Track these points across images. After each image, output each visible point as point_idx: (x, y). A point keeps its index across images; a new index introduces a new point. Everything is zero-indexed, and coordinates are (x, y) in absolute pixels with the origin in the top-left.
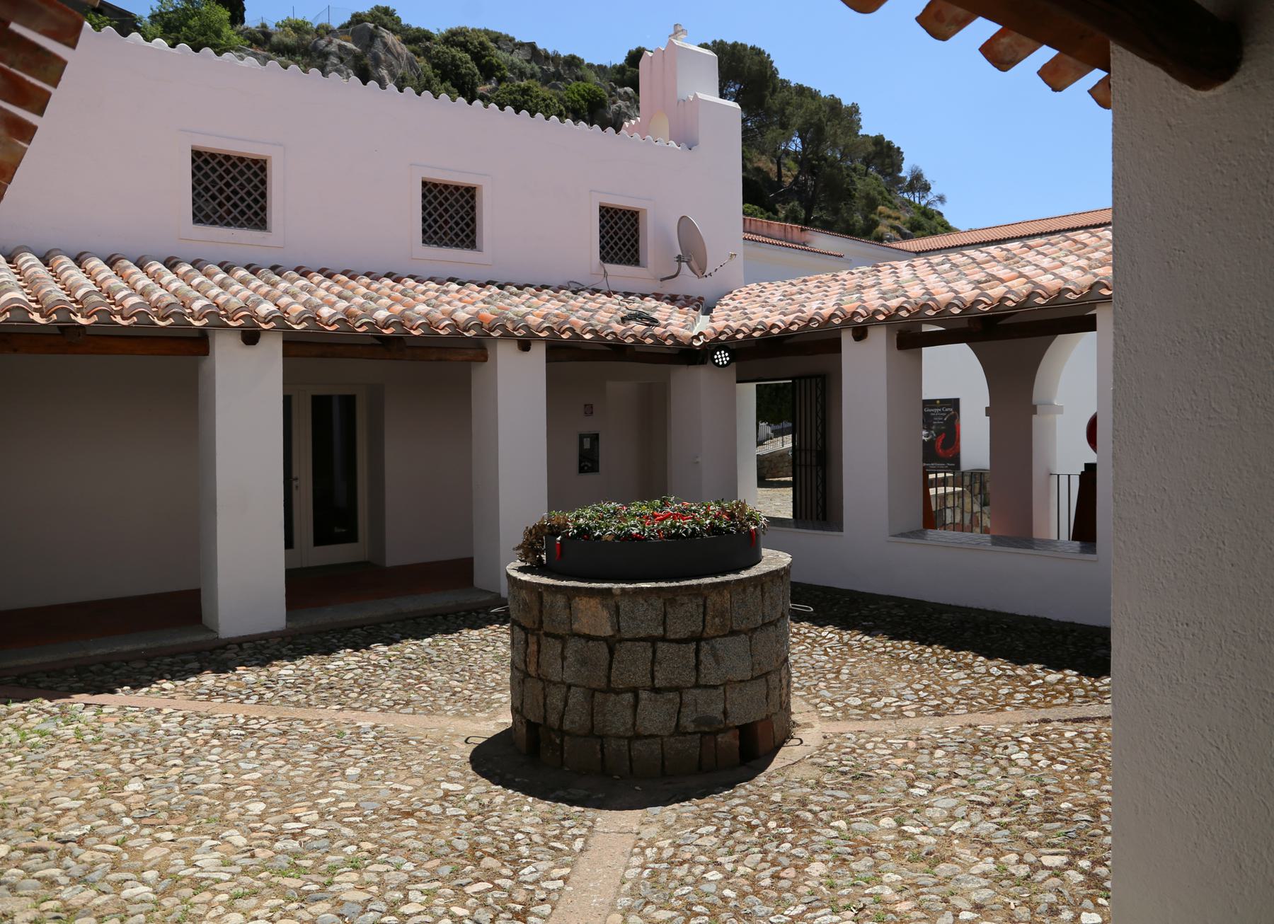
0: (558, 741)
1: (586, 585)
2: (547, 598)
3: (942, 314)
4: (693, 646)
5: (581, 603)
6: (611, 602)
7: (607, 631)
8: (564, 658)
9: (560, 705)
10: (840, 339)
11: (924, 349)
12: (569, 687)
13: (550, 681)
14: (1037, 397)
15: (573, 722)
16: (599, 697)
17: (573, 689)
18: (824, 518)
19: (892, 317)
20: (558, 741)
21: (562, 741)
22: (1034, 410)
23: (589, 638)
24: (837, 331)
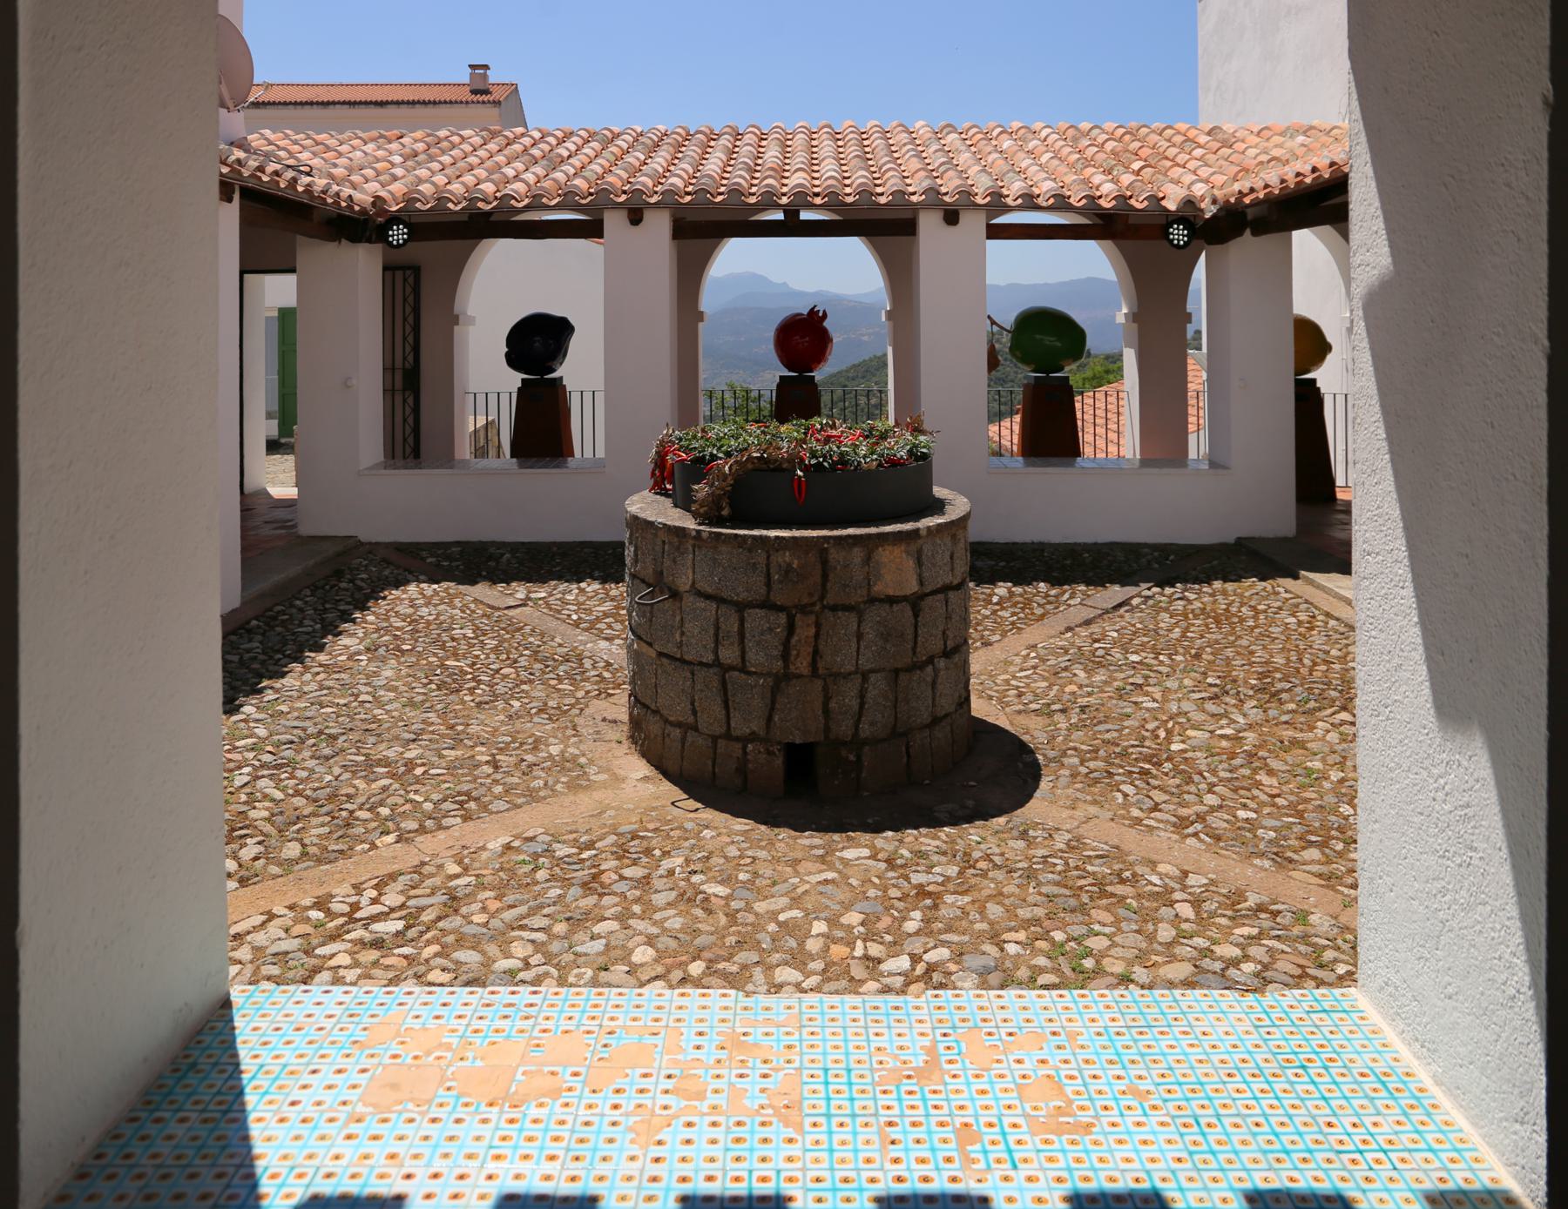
0: (852, 758)
1: (873, 530)
2: (835, 555)
3: (833, 201)
4: (830, 599)
5: (886, 555)
6: (913, 547)
7: (912, 587)
8: (860, 636)
9: (855, 704)
10: (601, 221)
11: (1294, 233)
12: (865, 676)
13: (837, 675)
14: (457, 309)
15: (872, 724)
16: (903, 677)
17: (873, 678)
18: (416, 453)
19: (669, 201)
20: (852, 758)
21: (859, 757)
22: (455, 320)
23: (892, 600)
24: (916, 208)
